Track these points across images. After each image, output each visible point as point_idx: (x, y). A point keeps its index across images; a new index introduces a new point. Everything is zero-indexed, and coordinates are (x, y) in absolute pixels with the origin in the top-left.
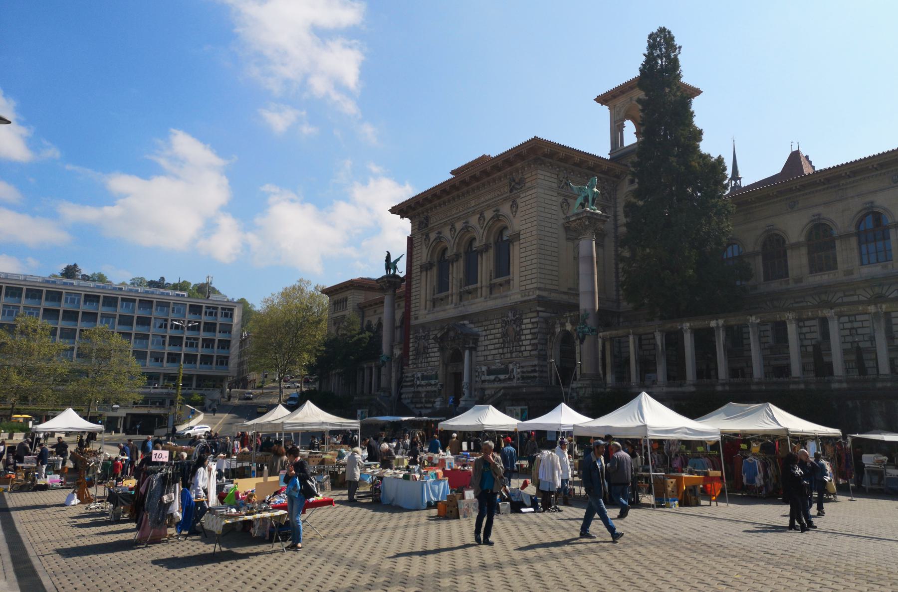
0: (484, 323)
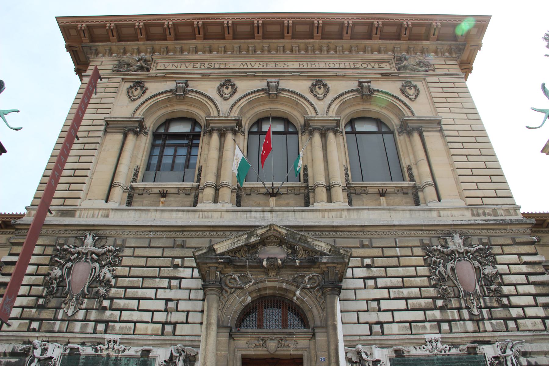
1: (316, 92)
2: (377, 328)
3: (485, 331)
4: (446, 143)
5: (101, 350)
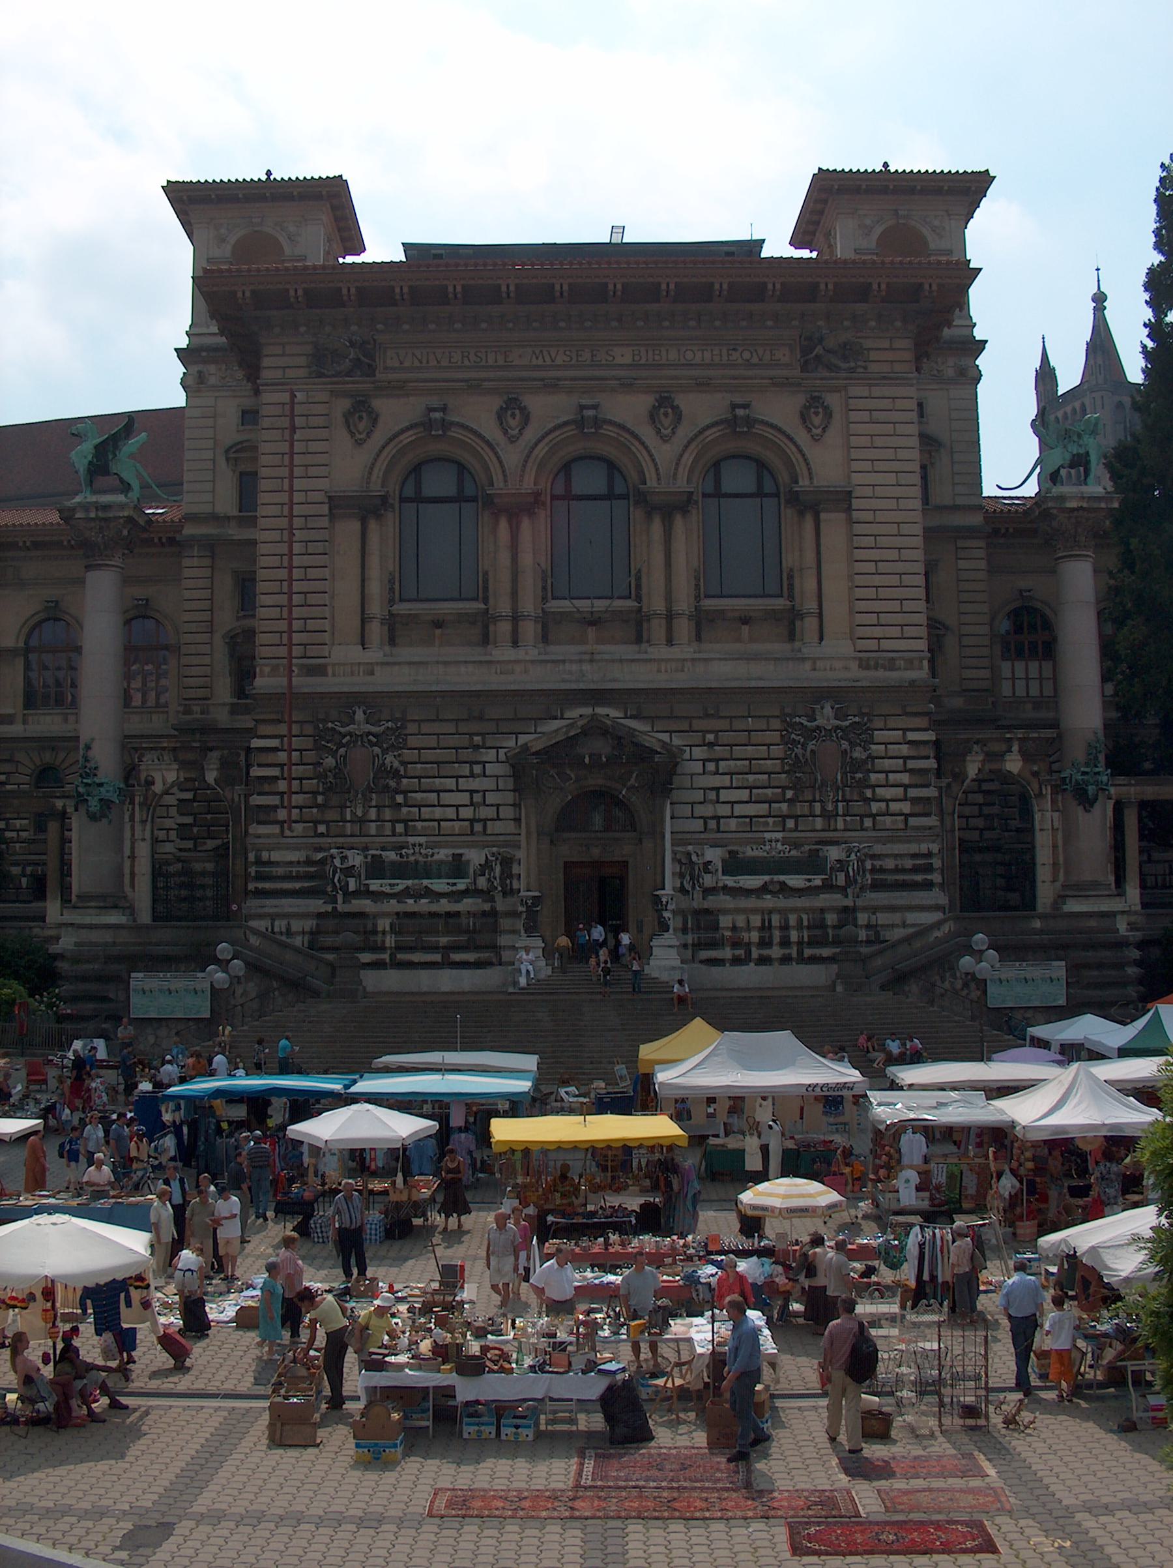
0: (698, 724)
1: (660, 422)
2: (712, 824)
3: (836, 830)
5: (407, 855)
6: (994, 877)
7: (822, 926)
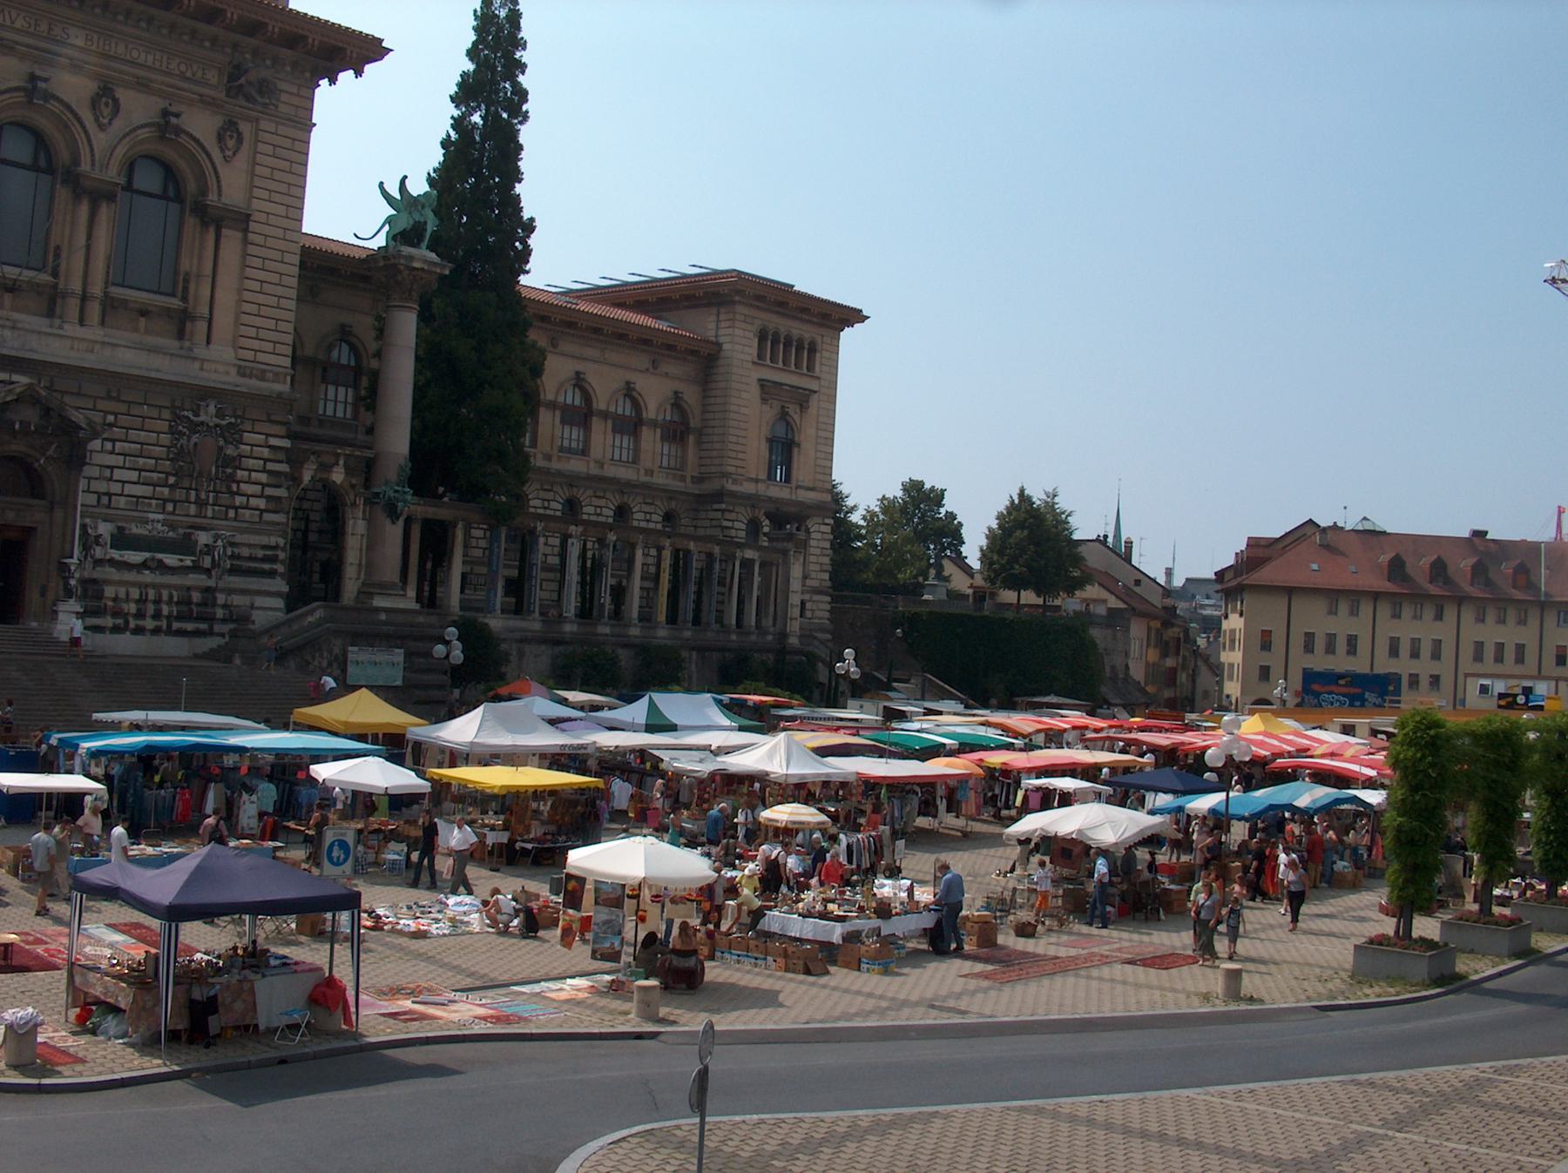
0: (101, 405)
2: (105, 500)
4: (245, 255)
6: (313, 566)
7: (189, 602)
